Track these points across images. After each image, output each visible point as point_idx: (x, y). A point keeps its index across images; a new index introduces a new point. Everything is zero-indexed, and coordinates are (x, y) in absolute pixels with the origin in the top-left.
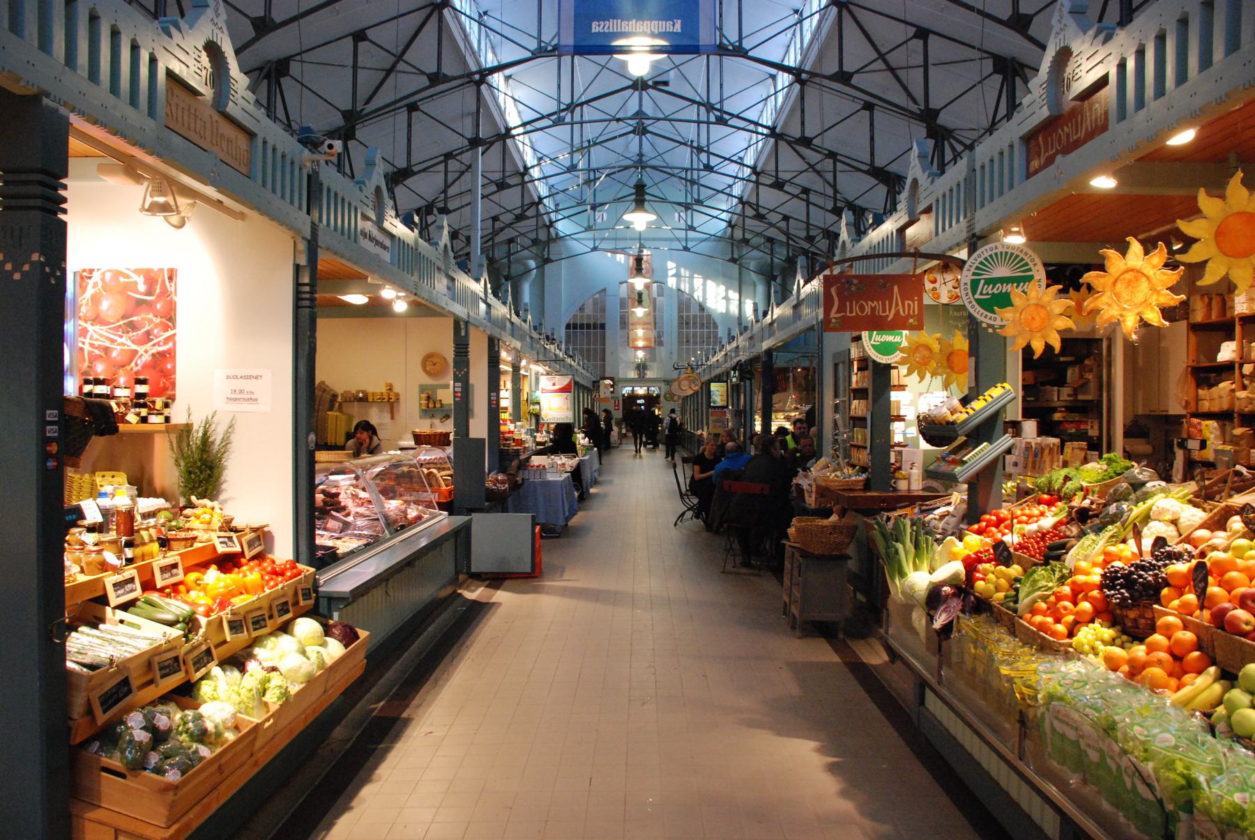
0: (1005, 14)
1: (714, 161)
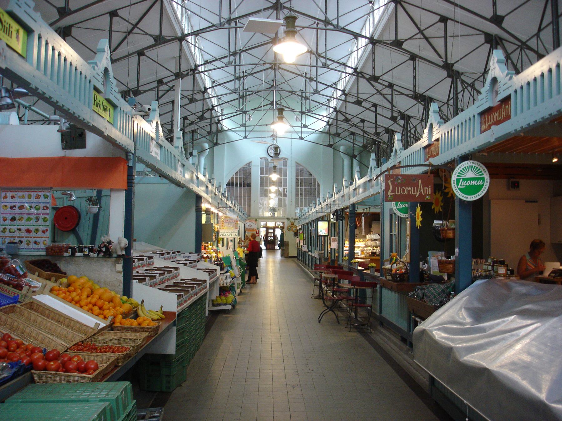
0: (489, 15)
1: (320, 87)
